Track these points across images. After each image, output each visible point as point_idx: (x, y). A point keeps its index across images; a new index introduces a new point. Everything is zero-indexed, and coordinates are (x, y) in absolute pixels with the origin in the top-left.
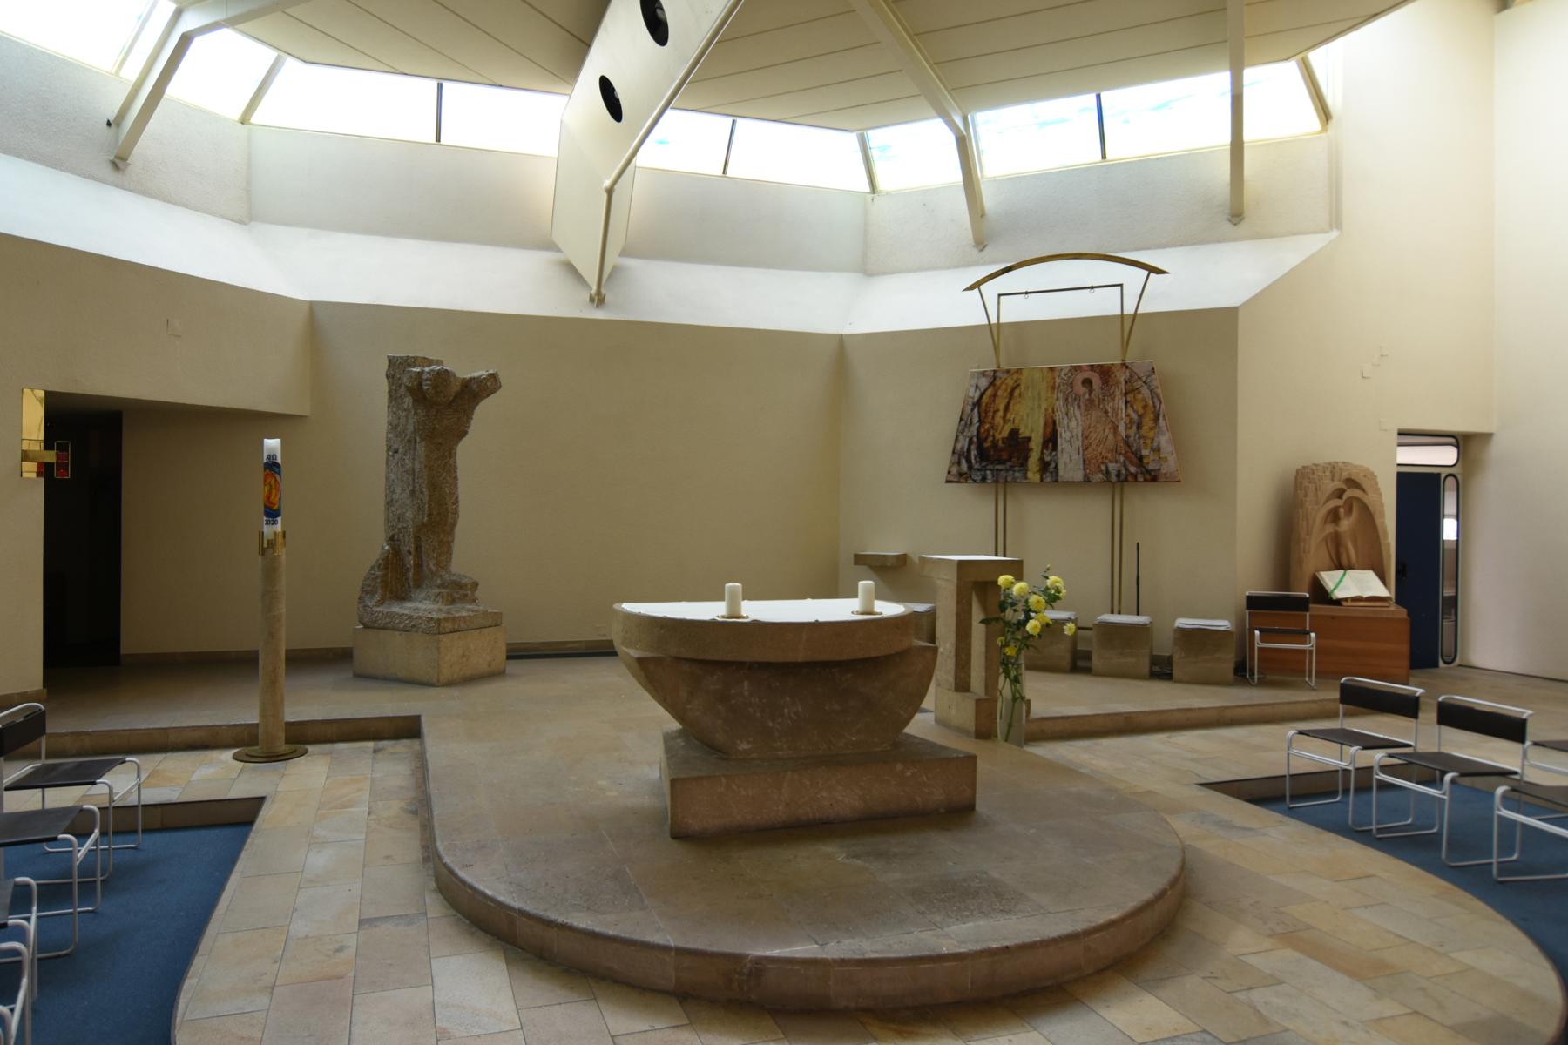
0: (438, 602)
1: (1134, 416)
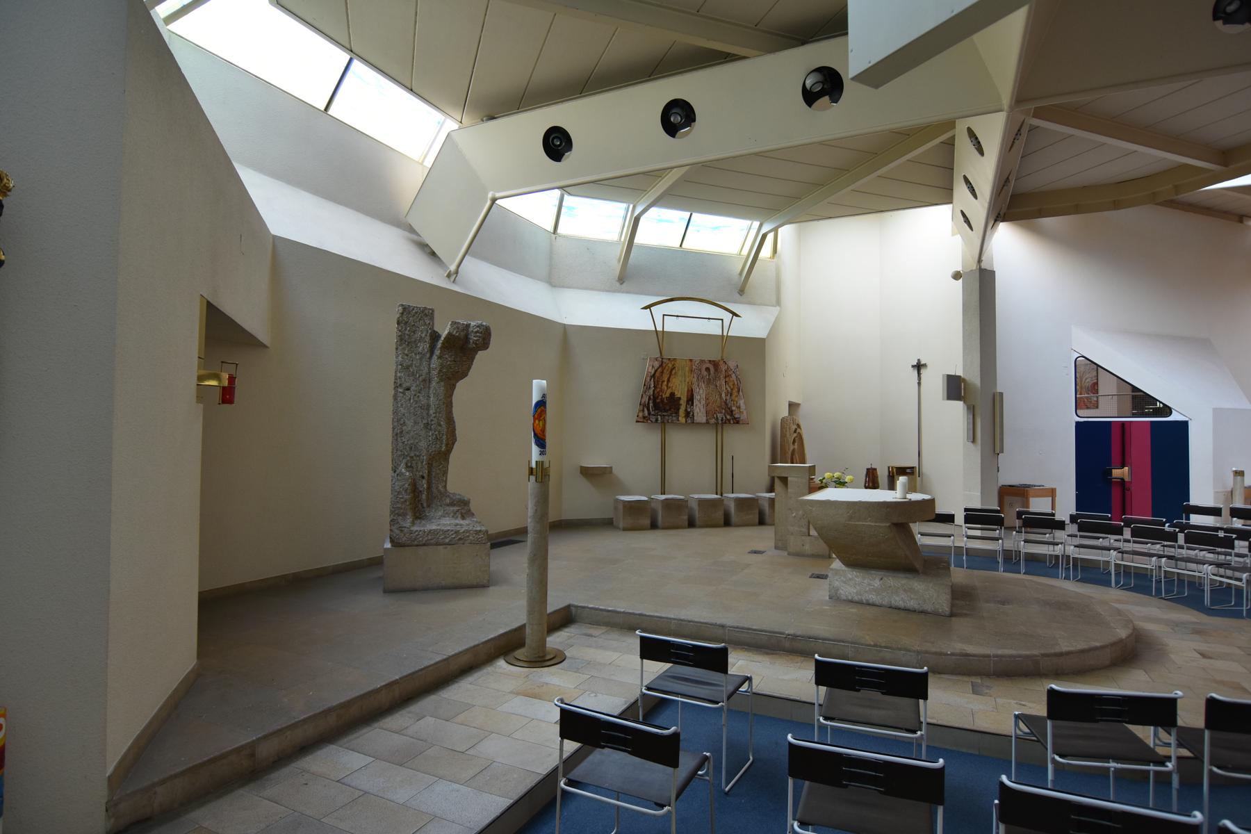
0: (457, 517)
1: (729, 389)
